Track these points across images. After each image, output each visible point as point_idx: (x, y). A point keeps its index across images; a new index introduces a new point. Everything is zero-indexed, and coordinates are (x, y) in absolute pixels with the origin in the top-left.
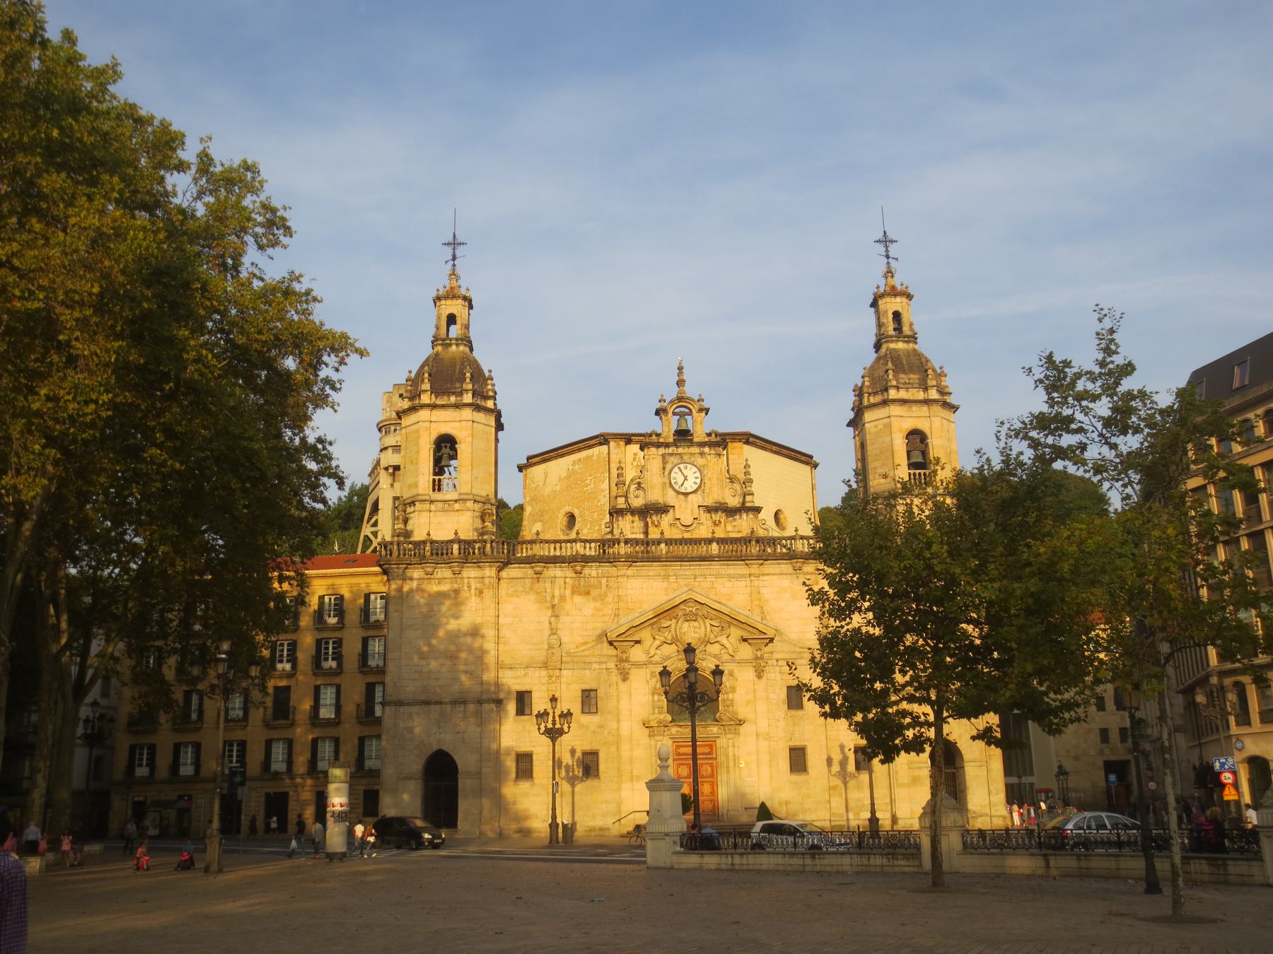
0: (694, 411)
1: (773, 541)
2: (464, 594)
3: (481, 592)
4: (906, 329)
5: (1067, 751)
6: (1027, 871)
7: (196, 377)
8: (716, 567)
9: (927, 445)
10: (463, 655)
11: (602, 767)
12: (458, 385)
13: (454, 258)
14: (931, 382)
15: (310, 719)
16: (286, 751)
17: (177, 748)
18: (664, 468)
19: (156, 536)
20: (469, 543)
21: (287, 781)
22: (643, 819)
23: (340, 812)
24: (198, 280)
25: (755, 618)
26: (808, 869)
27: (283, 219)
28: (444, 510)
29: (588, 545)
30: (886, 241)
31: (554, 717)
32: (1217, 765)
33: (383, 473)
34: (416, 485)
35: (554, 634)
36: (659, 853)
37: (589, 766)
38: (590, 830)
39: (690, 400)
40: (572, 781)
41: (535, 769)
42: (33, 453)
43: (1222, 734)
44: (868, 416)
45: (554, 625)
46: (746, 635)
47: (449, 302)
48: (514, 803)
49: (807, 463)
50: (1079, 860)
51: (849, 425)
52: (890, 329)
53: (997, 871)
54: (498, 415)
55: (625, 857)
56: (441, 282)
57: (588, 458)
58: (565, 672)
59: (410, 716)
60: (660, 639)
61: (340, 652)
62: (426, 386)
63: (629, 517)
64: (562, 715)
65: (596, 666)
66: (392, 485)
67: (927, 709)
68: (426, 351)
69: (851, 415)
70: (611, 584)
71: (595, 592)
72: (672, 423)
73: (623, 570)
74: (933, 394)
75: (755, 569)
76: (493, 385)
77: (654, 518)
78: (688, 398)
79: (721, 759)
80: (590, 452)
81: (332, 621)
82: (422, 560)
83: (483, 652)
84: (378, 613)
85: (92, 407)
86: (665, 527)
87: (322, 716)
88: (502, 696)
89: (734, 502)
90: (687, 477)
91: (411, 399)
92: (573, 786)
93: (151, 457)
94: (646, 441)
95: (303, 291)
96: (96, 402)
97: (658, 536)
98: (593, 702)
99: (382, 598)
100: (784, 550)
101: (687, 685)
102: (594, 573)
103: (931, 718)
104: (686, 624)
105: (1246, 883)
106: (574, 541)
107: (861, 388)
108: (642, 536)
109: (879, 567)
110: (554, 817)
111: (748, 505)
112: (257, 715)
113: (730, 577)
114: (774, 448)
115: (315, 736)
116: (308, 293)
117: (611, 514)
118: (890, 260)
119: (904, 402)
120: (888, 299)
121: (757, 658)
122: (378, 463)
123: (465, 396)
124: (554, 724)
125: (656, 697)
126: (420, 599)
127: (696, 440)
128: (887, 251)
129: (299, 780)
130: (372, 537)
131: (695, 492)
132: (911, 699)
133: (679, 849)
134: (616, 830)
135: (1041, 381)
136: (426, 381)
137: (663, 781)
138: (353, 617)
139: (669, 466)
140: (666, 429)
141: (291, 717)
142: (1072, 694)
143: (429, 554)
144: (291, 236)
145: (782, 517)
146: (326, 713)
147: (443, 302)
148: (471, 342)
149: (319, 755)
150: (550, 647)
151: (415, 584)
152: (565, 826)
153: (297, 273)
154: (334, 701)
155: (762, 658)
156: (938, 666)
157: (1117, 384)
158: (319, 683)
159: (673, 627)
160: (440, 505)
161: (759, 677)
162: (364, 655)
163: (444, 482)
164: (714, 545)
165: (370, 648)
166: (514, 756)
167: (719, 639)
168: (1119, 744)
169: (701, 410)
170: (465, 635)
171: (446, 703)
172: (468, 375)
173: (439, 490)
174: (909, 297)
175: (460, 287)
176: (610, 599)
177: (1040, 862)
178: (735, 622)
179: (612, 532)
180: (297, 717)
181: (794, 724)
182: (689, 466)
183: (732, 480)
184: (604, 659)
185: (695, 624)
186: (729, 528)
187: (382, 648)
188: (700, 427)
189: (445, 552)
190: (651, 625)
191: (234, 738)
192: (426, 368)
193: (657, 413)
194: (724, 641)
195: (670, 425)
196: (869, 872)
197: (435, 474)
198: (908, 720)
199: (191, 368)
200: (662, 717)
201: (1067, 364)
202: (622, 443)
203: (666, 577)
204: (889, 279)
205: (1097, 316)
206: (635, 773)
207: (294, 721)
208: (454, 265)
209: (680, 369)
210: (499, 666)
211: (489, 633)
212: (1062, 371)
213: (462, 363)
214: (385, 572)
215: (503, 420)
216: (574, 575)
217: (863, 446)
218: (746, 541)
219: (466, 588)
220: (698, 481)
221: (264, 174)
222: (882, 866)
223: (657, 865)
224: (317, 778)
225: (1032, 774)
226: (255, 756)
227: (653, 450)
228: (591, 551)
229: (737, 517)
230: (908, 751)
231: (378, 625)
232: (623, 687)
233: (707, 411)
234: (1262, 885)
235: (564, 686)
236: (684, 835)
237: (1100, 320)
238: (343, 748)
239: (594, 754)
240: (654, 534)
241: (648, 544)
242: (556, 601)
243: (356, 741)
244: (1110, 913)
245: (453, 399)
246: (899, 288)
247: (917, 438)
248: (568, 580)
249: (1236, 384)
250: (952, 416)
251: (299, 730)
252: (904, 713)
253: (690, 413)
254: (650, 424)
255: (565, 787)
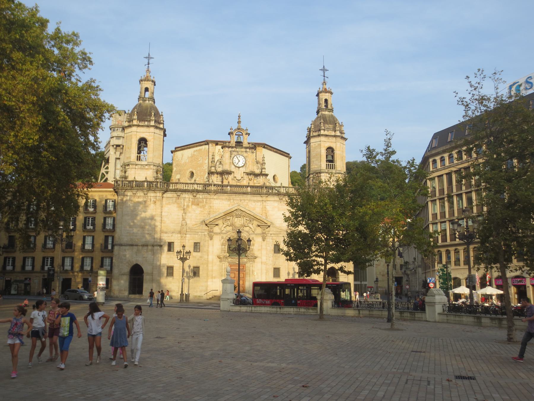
0: (244, 134)
1: (272, 188)
2: (148, 203)
3: (155, 202)
4: (329, 106)
5: (380, 272)
6: (352, 315)
7: (63, 126)
8: (249, 197)
9: (334, 153)
10: (147, 227)
11: (201, 273)
12: (148, 117)
13: (148, 64)
14: (337, 129)
15: (81, 249)
16: (71, 262)
17: (24, 259)
18: (231, 157)
19: (40, 182)
20: (151, 182)
21: (71, 274)
22: (218, 293)
23: (103, 288)
24: (64, 89)
25: (263, 218)
26: (278, 312)
27: (89, 58)
28: (141, 169)
29: (199, 185)
30: (324, 70)
31: (184, 253)
32: (428, 281)
33: (111, 148)
34: (130, 157)
35: (184, 220)
36: (226, 306)
37: (196, 272)
38: (195, 297)
39: (242, 129)
40: (189, 278)
41: (174, 273)
42: (9, 156)
43: (431, 269)
44: (312, 140)
45: (184, 217)
46: (259, 224)
47: (146, 82)
48: (166, 286)
49: (287, 157)
50: (370, 312)
51: (304, 143)
52: (323, 106)
53: (343, 315)
54: (165, 131)
55: (210, 307)
56: (143, 74)
57: (200, 150)
58: (188, 235)
59: (125, 250)
60: (226, 224)
61: (94, 223)
62: (135, 117)
63: (216, 175)
64: (187, 253)
65: (200, 233)
66: (115, 153)
67: (323, 260)
68: (135, 102)
69: (306, 139)
70: (207, 202)
71: (201, 204)
72: (234, 139)
73: (213, 196)
74: (338, 133)
75: (264, 198)
76: (163, 118)
77: (226, 176)
78: (242, 129)
79: (247, 271)
80: (201, 147)
81: (91, 210)
82: (132, 188)
83: (155, 226)
84: (110, 208)
85: (31, 141)
86: (230, 180)
87: (86, 248)
88: (162, 244)
89: (258, 171)
90: (240, 160)
91: (129, 122)
92: (189, 280)
93: (44, 155)
94: (224, 145)
95: (96, 86)
96: (33, 139)
97: (227, 183)
98: (198, 247)
99: (112, 201)
100: (276, 192)
101: (237, 245)
102: (201, 197)
103: (323, 263)
104: (236, 219)
105: (420, 320)
106: (194, 184)
107: (310, 129)
108: (220, 183)
109: (309, 211)
110: (182, 291)
111: (263, 173)
112: (58, 247)
113: (254, 201)
114: (275, 150)
115: (83, 256)
116: (97, 87)
117: (209, 174)
118: (325, 78)
119: (326, 136)
120: (323, 94)
121: (263, 233)
122: (109, 142)
123: (151, 122)
124: (183, 256)
125: (223, 247)
126: (130, 204)
127: (244, 146)
128: (324, 74)
129: (76, 274)
130: (105, 174)
131: (242, 167)
132: (317, 256)
133: (232, 304)
134: (205, 297)
135: (365, 155)
136: (136, 115)
137: (228, 280)
138: (100, 209)
139: (233, 156)
140: (232, 141)
141: (73, 248)
142: (370, 257)
143: (134, 186)
144: (92, 65)
145: (276, 177)
146: (88, 247)
147: (143, 82)
148: (154, 100)
149: (85, 264)
150: (182, 225)
151: (128, 198)
152: (186, 295)
153: (94, 79)
154: (91, 242)
155: (265, 233)
156: (327, 245)
157: (390, 157)
158: (85, 235)
159: (231, 219)
160: (139, 166)
161: (264, 240)
162: (104, 224)
163: (141, 157)
164: (249, 188)
165: (107, 221)
166: (166, 267)
167: (249, 225)
168: (400, 271)
169: (246, 134)
170: (148, 219)
171: (139, 246)
172: (153, 114)
173: (139, 160)
174: (331, 93)
175: (151, 76)
176: (207, 207)
177: (357, 312)
178: (255, 219)
179: (209, 181)
180: (75, 248)
181: (276, 259)
182: (241, 156)
183: (257, 163)
184: (203, 231)
185: (240, 219)
186: (255, 182)
187: (112, 222)
188: (246, 140)
189: (141, 185)
190: (223, 218)
191: (49, 256)
192: (136, 110)
193: (229, 134)
194: (251, 226)
195: (234, 139)
196: (300, 314)
197: (138, 153)
198: (315, 263)
199: (61, 123)
200: (225, 254)
201: (374, 150)
202: (214, 145)
203: (230, 200)
204: (324, 86)
205: (385, 133)
206: (214, 275)
207: (74, 250)
208: (148, 67)
209: (239, 116)
210: (162, 232)
211: (158, 218)
212: (372, 153)
213: (151, 108)
214: (116, 192)
215: (166, 133)
216: (193, 197)
217: (309, 152)
218: (262, 187)
219: (149, 200)
220: (244, 162)
221: (81, 38)
222: (304, 312)
223: (224, 310)
224: (84, 273)
225: (366, 281)
226: (58, 262)
227: (227, 149)
228: (200, 188)
229: (259, 177)
230: (315, 273)
231: (110, 212)
232: (210, 242)
233: (249, 134)
234: (425, 321)
235: (187, 241)
236: (234, 299)
237: (387, 135)
238: (94, 261)
239: (198, 268)
240: (225, 182)
241: (223, 186)
242: (185, 207)
243: (100, 259)
244: (373, 327)
245: (146, 123)
246: (328, 89)
247: (330, 150)
248: (190, 199)
249: (449, 140)
250: (345, 142)
251: (76, 254)
252: (314, 261)
253: (242, 135)
254: (227, 138)
255: (186, 280)
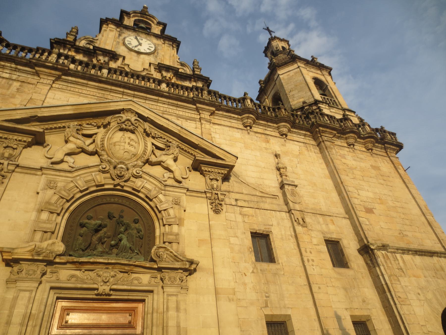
78: (149, 16)
185: (132, 136)
